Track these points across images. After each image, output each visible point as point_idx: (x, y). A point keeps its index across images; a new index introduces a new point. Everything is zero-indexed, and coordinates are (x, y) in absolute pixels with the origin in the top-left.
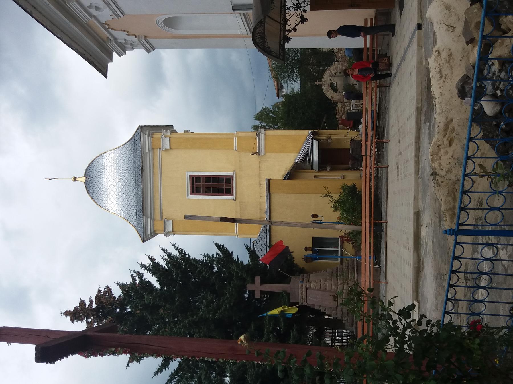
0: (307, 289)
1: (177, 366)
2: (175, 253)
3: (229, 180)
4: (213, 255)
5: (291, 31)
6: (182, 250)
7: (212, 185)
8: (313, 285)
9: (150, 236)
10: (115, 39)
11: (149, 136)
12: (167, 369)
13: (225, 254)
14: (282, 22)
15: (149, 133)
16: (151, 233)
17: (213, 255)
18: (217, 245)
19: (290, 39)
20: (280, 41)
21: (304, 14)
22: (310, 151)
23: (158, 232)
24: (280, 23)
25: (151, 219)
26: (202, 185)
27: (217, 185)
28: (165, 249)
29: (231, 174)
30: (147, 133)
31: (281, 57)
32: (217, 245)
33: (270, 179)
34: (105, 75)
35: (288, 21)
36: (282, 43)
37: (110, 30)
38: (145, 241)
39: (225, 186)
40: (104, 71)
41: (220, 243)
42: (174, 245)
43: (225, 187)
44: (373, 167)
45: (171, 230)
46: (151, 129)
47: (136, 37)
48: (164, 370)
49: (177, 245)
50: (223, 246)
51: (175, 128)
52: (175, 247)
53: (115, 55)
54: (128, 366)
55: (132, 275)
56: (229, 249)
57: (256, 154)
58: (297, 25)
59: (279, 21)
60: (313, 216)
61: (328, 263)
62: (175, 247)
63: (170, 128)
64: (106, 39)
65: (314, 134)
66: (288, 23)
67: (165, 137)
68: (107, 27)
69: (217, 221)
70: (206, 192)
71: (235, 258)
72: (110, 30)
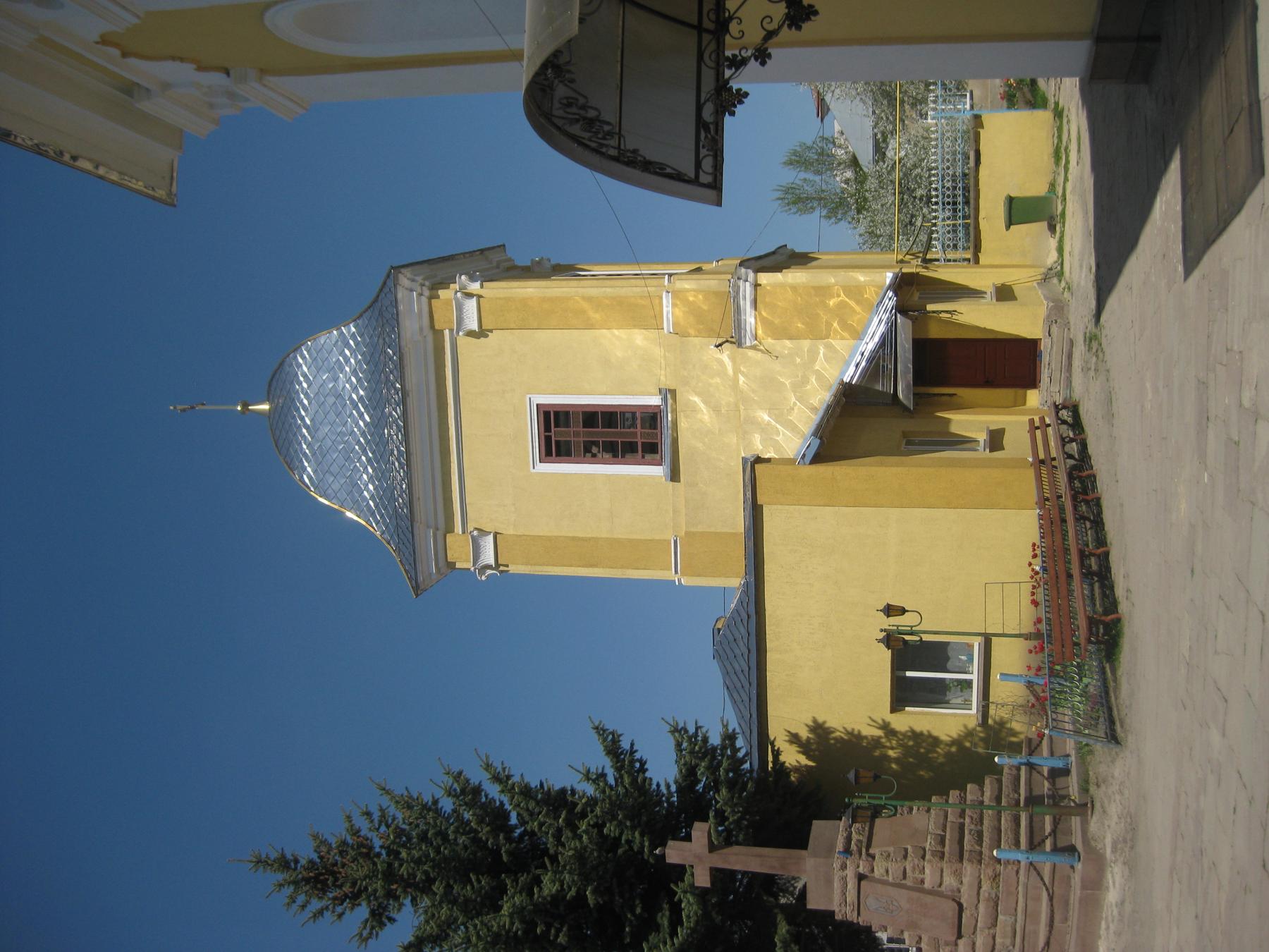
0: (861, 878)
3: (652, 418)
5: (744, 62)
8: (878, 873)
14: (707, 24)
19: (741, 96)
20: (699, 108)
22: (887, 351)
24: (699, 28)
29: (655, 401)
31: (705, 179)
33: (758, 460)
35: (731, 18)
36: (708, 113)
39: (640, 435)
44: (1111, 931)
45: (492, 561)
47: (228, 74)
58: (770, 35)
59: (694, 20)
60: (890, 610)
61: (943, 680)
66: (734, 27)
67: (469, 295)
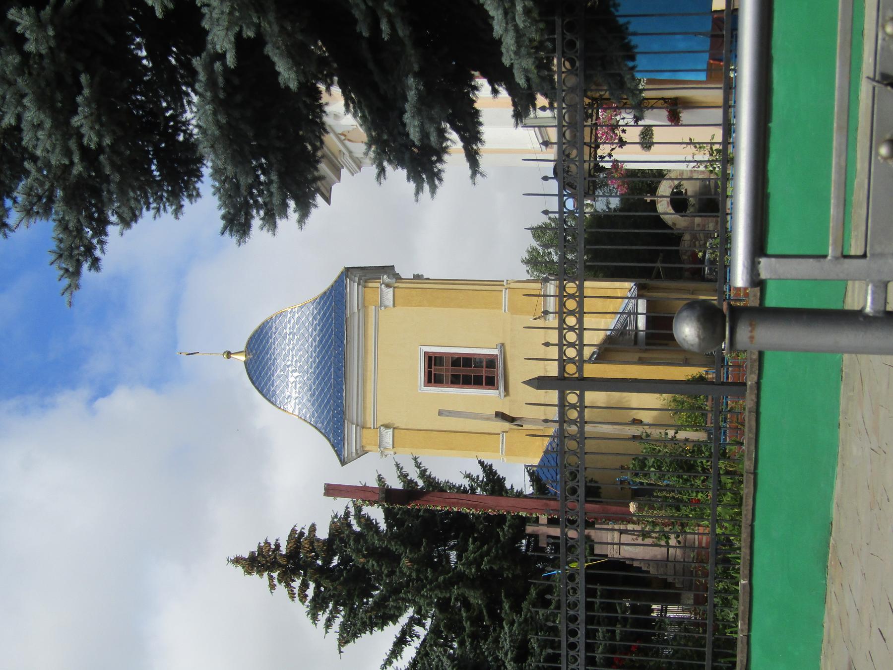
1: (414, 655)
2: (414, 475)
3: (491, 362)
4: (478, 477)
6: (425, 470)
7: (462, 371)
9: (354, 455)
10: (350, 152)
11: (359, 284)
12: (399, 658)
13: (494, 482)
15: (360, 279)
16: (356, 450)
17: (478, 477)
18: (481, 463)
21: (622, 135)
23: (367, 448)
25: (357, 425)
26: (446, 370)
27: (471, 372)
28: (401, 466)
29: (495, 352)
30: (357, 279)
32: (481, 463)
34: (329, 203)
37: (347, 142)
38: (346, 463)
39: (484, 372)
40: (327, 195)
41: (487, 461)
42: (415, 459)
43: (484, 374)
46: (360, 273)
48: (394, 660)
49: (419, 460)
50: (491, 466)
51: (397, 270)
52: (416, 462)
53: (344, 172)
54: (340, 652)
55: (347, 508)
56: (499, 473)
57: (539, 318)
62: (416, 462)
63: (388, 270)
64: (337, 153)
65: (641, 287)
68: (343, 138)
69: (488, 419)
70: (452, 383)
71: (508, 486)
72: (347, 142)
